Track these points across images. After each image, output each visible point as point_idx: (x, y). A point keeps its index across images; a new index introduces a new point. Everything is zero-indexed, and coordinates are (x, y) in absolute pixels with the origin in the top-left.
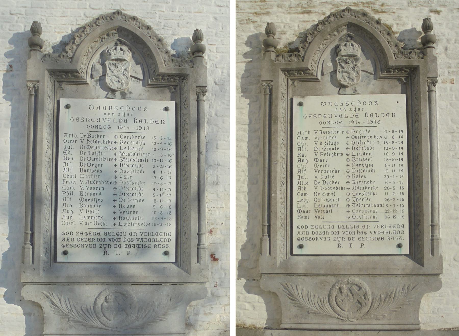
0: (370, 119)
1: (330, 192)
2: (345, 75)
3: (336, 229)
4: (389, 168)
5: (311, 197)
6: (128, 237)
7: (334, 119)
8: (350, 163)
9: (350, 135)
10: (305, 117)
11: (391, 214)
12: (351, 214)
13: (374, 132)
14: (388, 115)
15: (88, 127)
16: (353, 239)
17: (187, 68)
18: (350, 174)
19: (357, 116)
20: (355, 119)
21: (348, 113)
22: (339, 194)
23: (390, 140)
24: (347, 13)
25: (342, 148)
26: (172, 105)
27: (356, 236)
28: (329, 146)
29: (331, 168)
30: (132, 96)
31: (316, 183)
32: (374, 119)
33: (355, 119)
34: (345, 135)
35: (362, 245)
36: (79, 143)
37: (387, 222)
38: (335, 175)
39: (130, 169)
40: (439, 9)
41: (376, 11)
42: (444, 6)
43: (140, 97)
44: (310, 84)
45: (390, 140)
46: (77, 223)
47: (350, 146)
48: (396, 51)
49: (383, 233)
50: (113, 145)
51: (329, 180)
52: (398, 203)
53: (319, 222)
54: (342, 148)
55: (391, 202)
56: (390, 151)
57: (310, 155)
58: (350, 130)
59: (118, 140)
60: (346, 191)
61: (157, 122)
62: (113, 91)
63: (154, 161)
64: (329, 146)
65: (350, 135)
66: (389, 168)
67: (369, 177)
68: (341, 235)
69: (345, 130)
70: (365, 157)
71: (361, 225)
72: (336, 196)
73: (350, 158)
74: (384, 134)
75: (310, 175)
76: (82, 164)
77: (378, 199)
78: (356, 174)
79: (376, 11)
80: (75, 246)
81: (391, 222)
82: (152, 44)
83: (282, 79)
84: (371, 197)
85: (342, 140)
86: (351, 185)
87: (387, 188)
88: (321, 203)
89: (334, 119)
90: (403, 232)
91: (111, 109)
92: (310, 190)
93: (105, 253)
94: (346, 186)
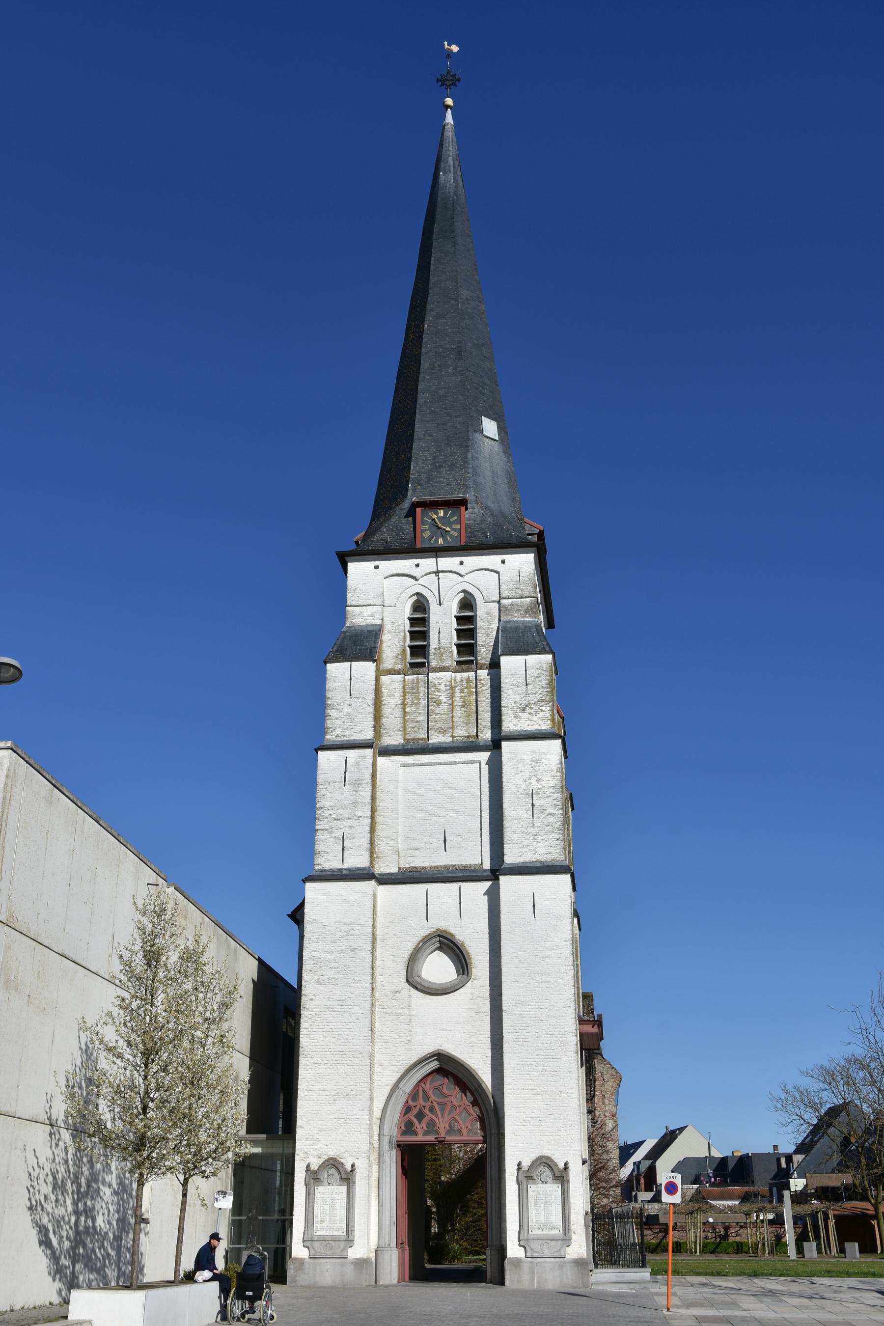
13: (337, 1198)
17: (564, 1174)
24: (331, 1161)
25: (328, 1203)
26: (560, 1185)
37: (340, 1225)
41: (340, 1158)
53: (321, 1225)
54: (328, 1203)
62: (543, 1182)
75: (319, 1211)
77: (337, 1218)
79: (340, 1158)
82: (553, 1167)
83: (312, 1181)
85: (328, 1200)
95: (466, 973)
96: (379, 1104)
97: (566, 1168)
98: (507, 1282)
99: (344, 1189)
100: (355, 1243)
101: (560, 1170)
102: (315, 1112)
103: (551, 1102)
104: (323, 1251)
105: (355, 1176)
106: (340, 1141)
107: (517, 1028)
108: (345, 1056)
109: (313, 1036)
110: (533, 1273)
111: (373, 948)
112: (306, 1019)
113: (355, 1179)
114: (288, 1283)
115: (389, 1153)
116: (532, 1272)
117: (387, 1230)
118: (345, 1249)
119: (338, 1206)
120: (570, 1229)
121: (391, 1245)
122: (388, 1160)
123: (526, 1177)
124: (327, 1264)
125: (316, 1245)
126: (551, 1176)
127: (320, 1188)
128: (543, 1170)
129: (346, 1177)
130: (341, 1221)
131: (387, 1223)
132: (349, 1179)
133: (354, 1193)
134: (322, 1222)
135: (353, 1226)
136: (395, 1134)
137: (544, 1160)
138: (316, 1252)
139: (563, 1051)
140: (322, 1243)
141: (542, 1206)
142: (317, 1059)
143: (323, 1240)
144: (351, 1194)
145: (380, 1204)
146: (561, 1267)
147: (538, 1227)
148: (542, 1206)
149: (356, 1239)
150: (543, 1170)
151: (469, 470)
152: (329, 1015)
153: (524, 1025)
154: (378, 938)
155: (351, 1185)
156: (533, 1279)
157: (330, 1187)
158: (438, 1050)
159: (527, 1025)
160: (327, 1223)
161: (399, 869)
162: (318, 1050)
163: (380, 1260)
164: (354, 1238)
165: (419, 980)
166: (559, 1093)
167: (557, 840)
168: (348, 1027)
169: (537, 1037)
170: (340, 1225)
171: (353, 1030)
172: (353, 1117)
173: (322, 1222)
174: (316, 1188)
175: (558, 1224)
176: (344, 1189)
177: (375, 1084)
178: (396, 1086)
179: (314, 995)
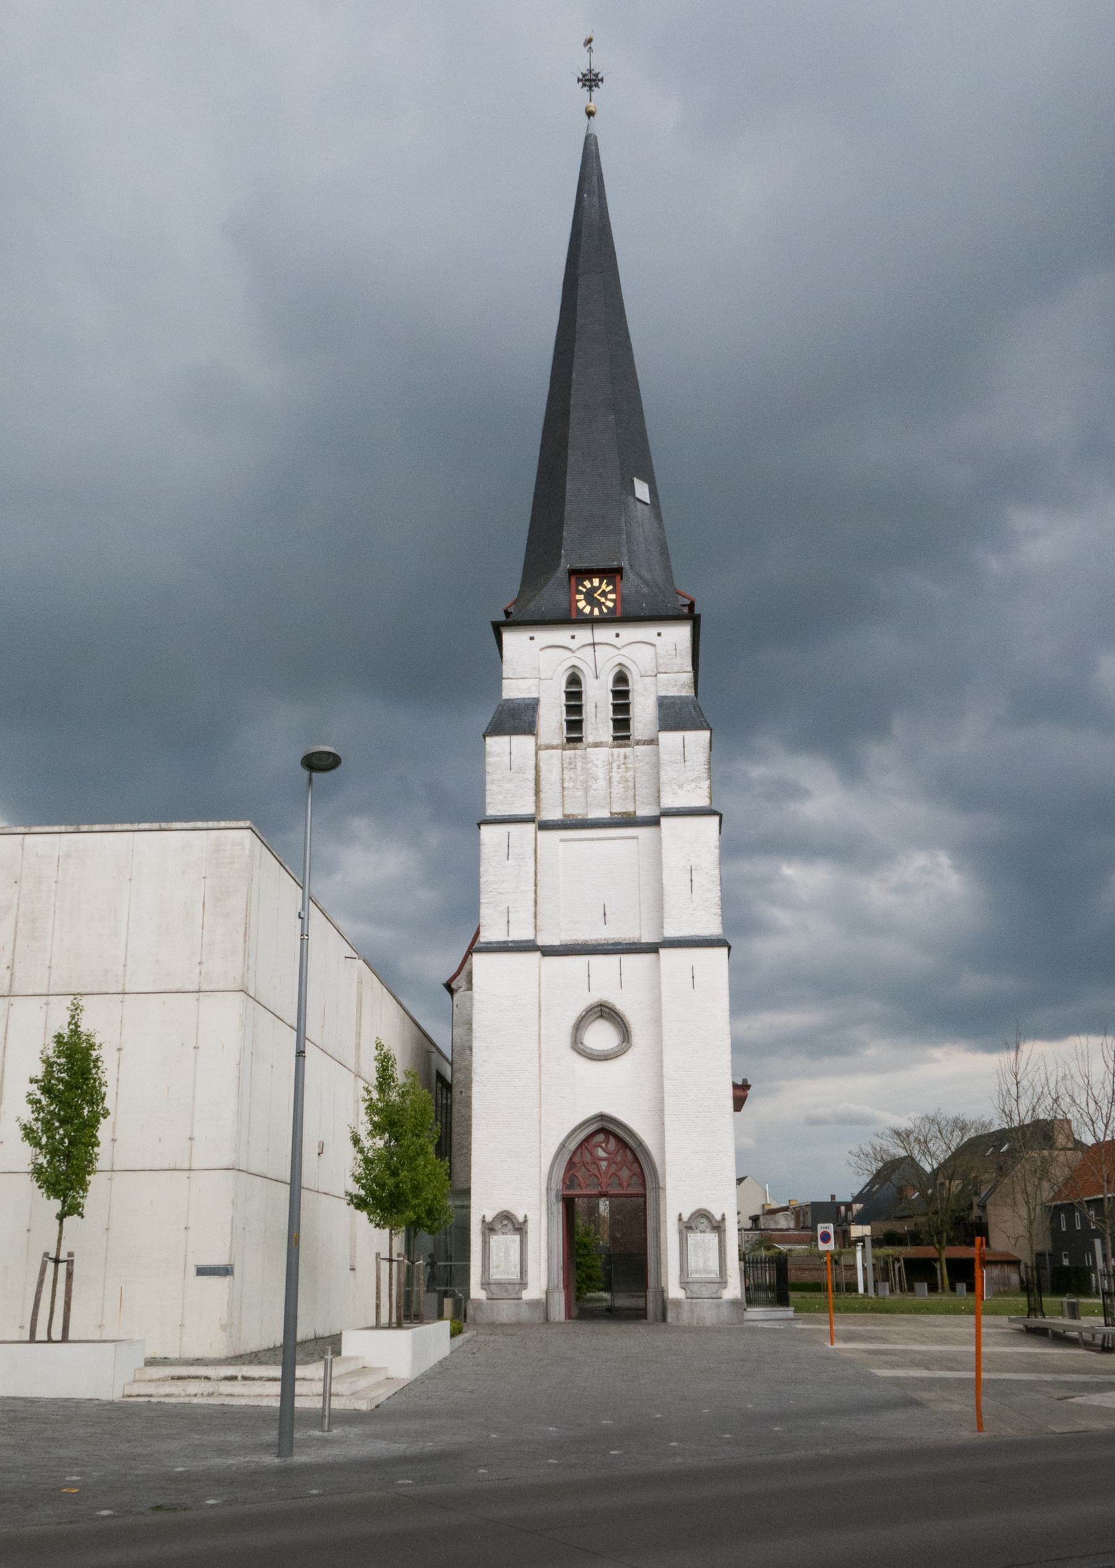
57: (495, 1252)
75: (494, 1257)
96: (546, 1169)
97: (723, 1219)
98: (669, 1320)
99: (517, 1238)
100: (529, 1286)
101: (717, 1221)
116: (692, 1311)
118: (520, 1291)
119: (512, 1253)
120: (726, 1274)
122: (555, 1212)
124: (504, 1304)
125: (493, 1287)
128: (702, 1221)
129: (518, 1226)
130: (515, 1266)
131: (556, 1268)
133: (527, 1242)
134: (497, 1267)
135: (526, 1271)
138: (493, 1294)
141: (700, 1253)
143: (499, 1284)
147: (697, 1271)
148: (700, 1253)
149: (529, 1282)
150: (702, 1221)
160: (502, 1268)
161: (561, 941)
163: (551, 1301)
167: (715, 914)
173: (497, 1267)
176: (517, 1238)
178: (563, 1146)
179: (484, 1061)
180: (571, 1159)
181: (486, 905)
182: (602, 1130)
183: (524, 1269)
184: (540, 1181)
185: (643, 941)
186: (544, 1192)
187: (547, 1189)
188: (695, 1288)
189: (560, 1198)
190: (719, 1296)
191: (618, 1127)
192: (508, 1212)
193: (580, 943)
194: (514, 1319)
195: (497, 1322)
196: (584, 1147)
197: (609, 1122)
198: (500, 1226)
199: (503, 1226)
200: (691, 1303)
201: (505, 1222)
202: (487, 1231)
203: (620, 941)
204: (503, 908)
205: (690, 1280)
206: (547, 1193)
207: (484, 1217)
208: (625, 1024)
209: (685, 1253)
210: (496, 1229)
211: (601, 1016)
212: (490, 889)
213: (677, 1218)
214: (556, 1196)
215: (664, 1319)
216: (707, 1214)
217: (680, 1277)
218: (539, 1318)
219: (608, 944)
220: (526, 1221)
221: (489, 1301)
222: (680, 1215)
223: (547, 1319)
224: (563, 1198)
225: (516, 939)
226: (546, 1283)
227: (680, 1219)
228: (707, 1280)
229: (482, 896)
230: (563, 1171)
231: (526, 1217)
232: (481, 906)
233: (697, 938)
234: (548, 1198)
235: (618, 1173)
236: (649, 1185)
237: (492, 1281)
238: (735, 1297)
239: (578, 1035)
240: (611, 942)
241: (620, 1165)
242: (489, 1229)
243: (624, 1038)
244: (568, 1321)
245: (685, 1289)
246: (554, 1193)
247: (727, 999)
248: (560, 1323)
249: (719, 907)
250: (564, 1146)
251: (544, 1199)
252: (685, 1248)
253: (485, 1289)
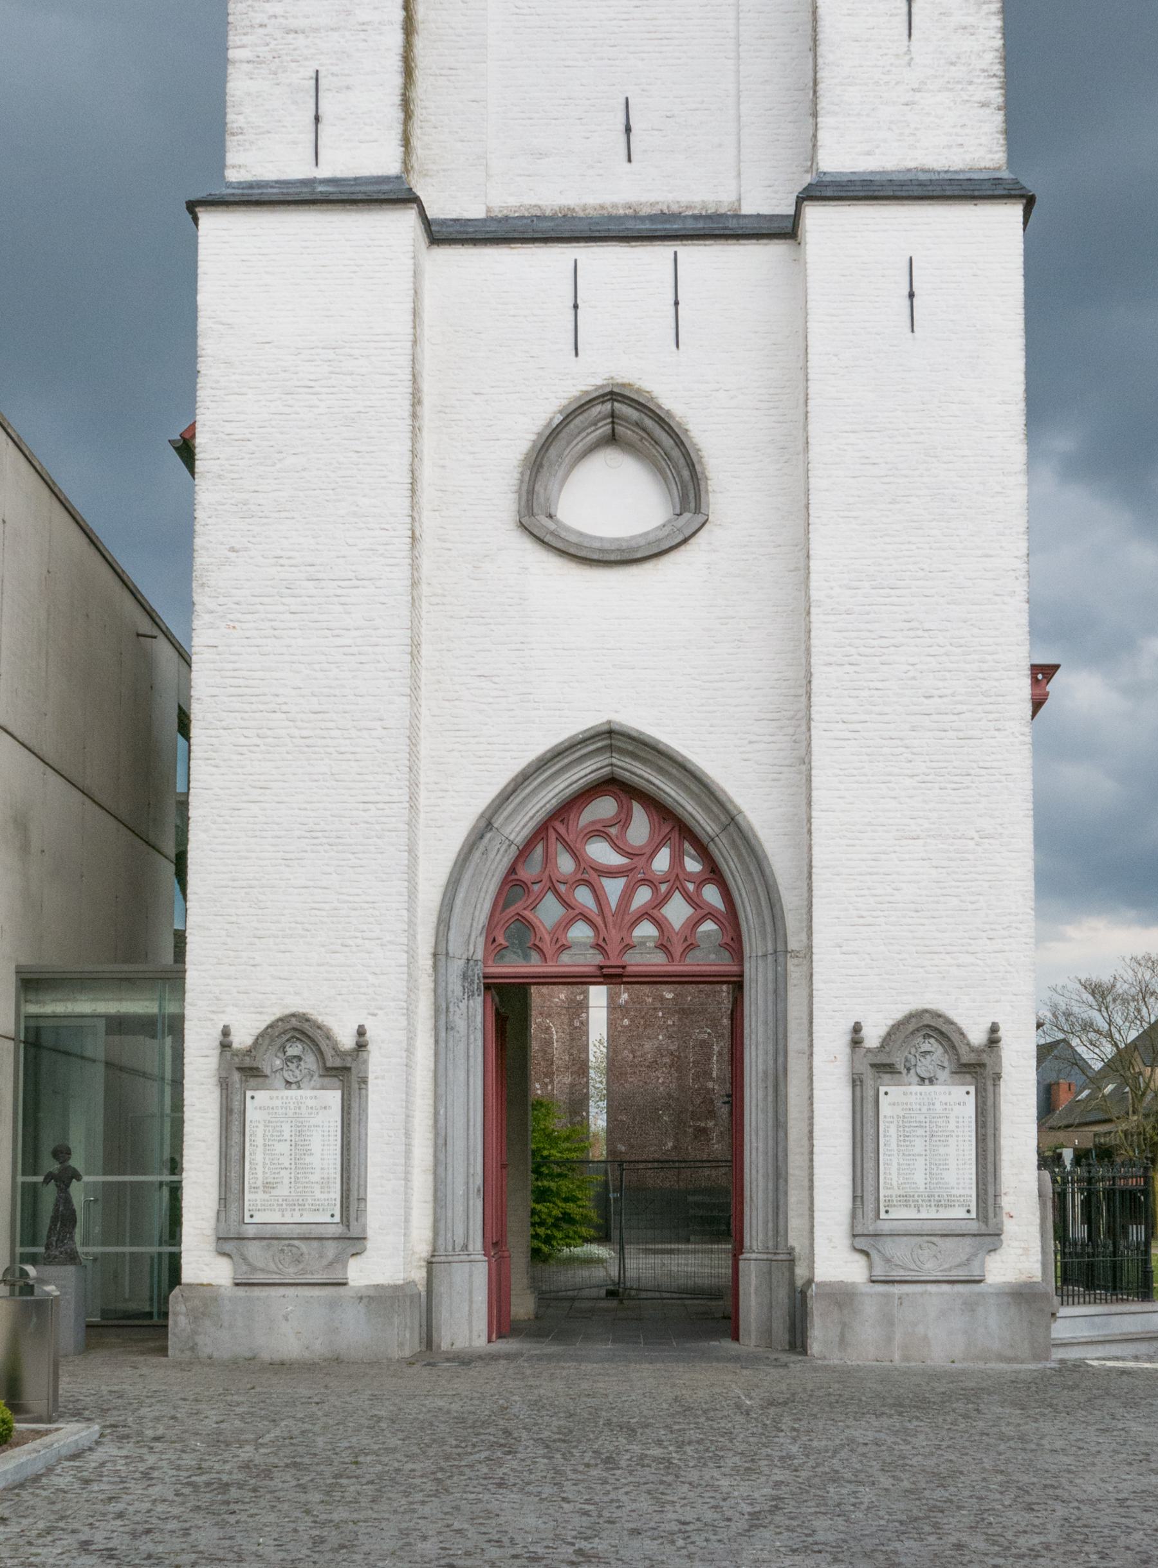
0: (310, 1111)
1: (277, 1171)
2: (290, 1073)
3: (280, 1202)
4: (325, 1152)
5: (260, 1175)
6: (937, 1198)
7: (280, 1111)
8: (293, 1148)
9: (293, 1124)
10: (256, 1108)
11: (326, 1190)
12: (293, 1189)
14: (325, 1108)
15: (903, 1109)
16: (930, 1206)
17: (985, 1058)
18: (293, 1157)
19: (300, 1108)
20: (298, 1111)
21: (292, 1106)
22: (284, 1173)
23: (326, 1129)
24: (293, 1019)
25: (287, 1135)
26: (972, 1089)
27: (297, 1208)
28: (275, 1134)
29: (277, 1152)
30: (939, 1082)
31: (264, 1164)
32: (314, 1111)
33: (298, 1111)
34: (289, 1124)
35: (301, 1215)
36: (896, 1123)
37: (322, 1196)
38: (281, 1157)
39: (938, 1143)
40: (376, 1011)
42: (381, 1009)
43: (945, 1083)
44: (897, 1075)
45: (326, 1129)
46: (896, 1188)
47: (293, 1133)
48: (333, 1053)
49: (954, 1201)
50: (924, 1124)
51: (276, 1162)
52: (332, 1180)
53: (266, 1196)
54: (287, 1135)
55: (326, 1180)
56: (326, 1138)
57: (259, 1141)
58: (294, 1120)
59: (928, 1120)
60: (289, 1171)
61: (959, 1104)
62: (923, 1079)
63: (958, 1136)
64: (275, 1134)
65: (293, 1124)
66: (325, 1152)
67: (308, 1159)
68: (284, 1207)
69: (290, 1120)
70: (306, 1143)
71: (301, 1199)
72: (281, 1175)
73: (293, 1143)
74: (321, 1124)
75: (259, 1157)
76: (899, 1141)
77: (315, 1178)
78: (298, 1157)
80: (895, 1206)
81: (326, 1196)
82: (955, 1038)
84: (310, 1176)
86: (293, 1166)
87: (322, 1169)
88: (269, 1181)
89: (280, 1111)
90: (335, 1205)
91: (921, 1094)
92: (260, 1170)
93: (919, 1211)
94: (289, 1166)
95: (692, 505)
96: (430, 895)
97: (993, 1041)
98: (815, 1347)
99: (334, 1097)
100: (369, 1244)
101: (973, 1049)
102: (244, 883)
103: (951, 860)
104: (272, 1267)
105: (365, 1062)
106: (319, 965)
107: (853, 651)
108: (331, 725)
109: (231, 666)
110: (891, 1324)
111: (415, 432)
112: (207, 618)
113: (366, 1071)
114: (170, 1353)
115: (463, 1005)
116: (888, 1321)
117: (460, 1208)
118: (340, 1261)
119: (316, 1145)
120: (997, 1207)
121: (471, 1248)
122: (461, 1024)
123: (873, 1066)
124: (285, 1301)
125: (254, 1251)
126: (946, 1064)
127: (262, 1096)
128: (926, 1047)
129: (338, 1063)
130: (325, 1184)
131: (460, 1191)
132: (348, 1069)
133: (364, 1110)
134: (268, 1187)
135: (362, 1200)
136: (479, 955)
137: (927, 1020)
138: (254, 1269)
139: (991, 717)
140: (269, 1246)
141: (919, 1146)
142: (245, 732)
143: (271, 1238)
144: (355, 1110)
145: (441, 1141)
146: (970, 1306)
147: (906, 1200)
148: (919, 1146)
149: (370, 1233)
150: (926, 1047)
151: (356, 1557)
152: (281, 608)
153: (875, 643)
154: (427, 400)
155: (355, 1086)
156: (889, 1340)
157: (292, 1093)
158: (609, 722)
159: (884, 642)
160: (283, 1191)
161: (489, 210)
162: (247, 707)
163: (441, 1288)
164: (364, 1230)
165: (551, 525)
166: (976, 835)
167: (984, 105)
168: (339, 641)
169: (914, 678)
170: (322, 1196)
171: (354, 650)
172: (357, 899)
173: (268, 1187)
174: (249, 1094)
175: (961, 1192)
176: (334, 1097)
177: (422, 815)
178: (486, 825)
179: (232, 549)
180: (512, 870)
181: (246, 67)
182: (611, 785)
183: (354, 1195)
184: (411, 923)
185: (746, 210)
186: (425, 962)
187: (435, 955)
188: (898, 1250)
189: (478, 984)
190: (976, 1273)
191: (661, 771)
192: (304, 1018)
193: (548, 213)
194: (319, 1348)
195: (266, 1356)
196: (552, 836)
197: (634, 756)
198: (278, 1063)
199: (289, 1060)
200: (886, 1296)
201: (294, 1050)
202: (236, 1076)
203: (675, 208)
204: (301, 76)
205: (885, 1227)
206: (435, 967)
207: (226, 1032)
208: (686, 455)
209: (869, 1146)
210: (268, 1072)
211: (612, 439)
212: (259, 18)
213: (847, 1038)
214: (465, 976)
215: (797, 1342)
216: (944, 1028)
217: (854, 1215)
218: (401, 1345)
219: (636, 217)
220: (361, 1046)
221: (241, 1292)
222: (857, 1029)
223: (429, 1341)
224: (487, 987)
225: (339, 174)
226: (428, 1234)
227: (856, 1042)
228: (938, 1227)
229: (233, 39)
230: (487, 906)
231: (361, 1032)
232: (231, 69)
233: (923, 177)
234: (436, 982)
235: (655, 913)
236: (754, 943)
237: (250, 1231)
238: (1023, 1278)
239: (538, 488)
240: (645, 211)
241: (663, 888)
242: (239, 1069)
243: (684, 499)
244: (503, 1346)
245: (866, 1254)
246: (457, 966)
247: (1019, 363)
248: (465, 1360)
249: (996, 82)
250: (489, 825)
251: (425, 982)
252: (869, 1130)
253: (228, 1255)
